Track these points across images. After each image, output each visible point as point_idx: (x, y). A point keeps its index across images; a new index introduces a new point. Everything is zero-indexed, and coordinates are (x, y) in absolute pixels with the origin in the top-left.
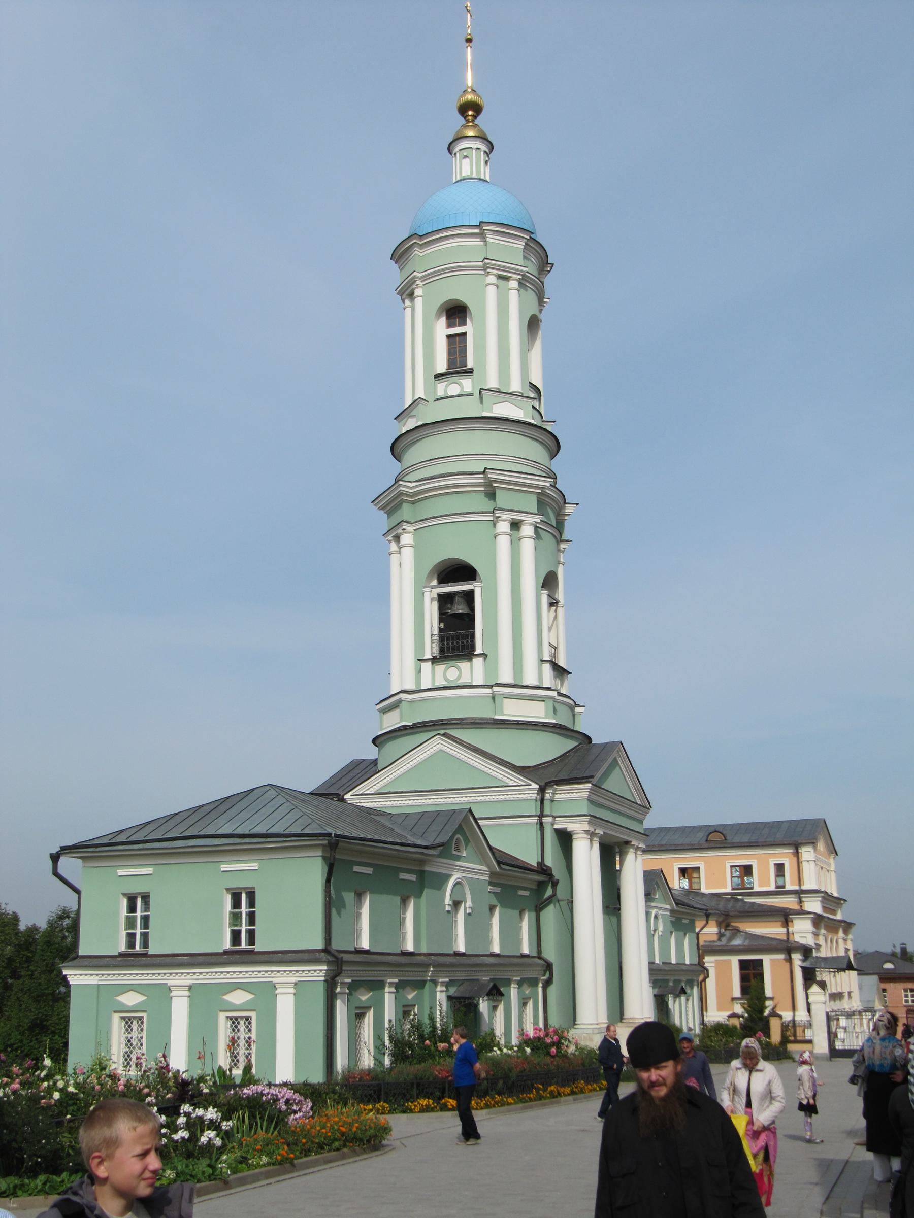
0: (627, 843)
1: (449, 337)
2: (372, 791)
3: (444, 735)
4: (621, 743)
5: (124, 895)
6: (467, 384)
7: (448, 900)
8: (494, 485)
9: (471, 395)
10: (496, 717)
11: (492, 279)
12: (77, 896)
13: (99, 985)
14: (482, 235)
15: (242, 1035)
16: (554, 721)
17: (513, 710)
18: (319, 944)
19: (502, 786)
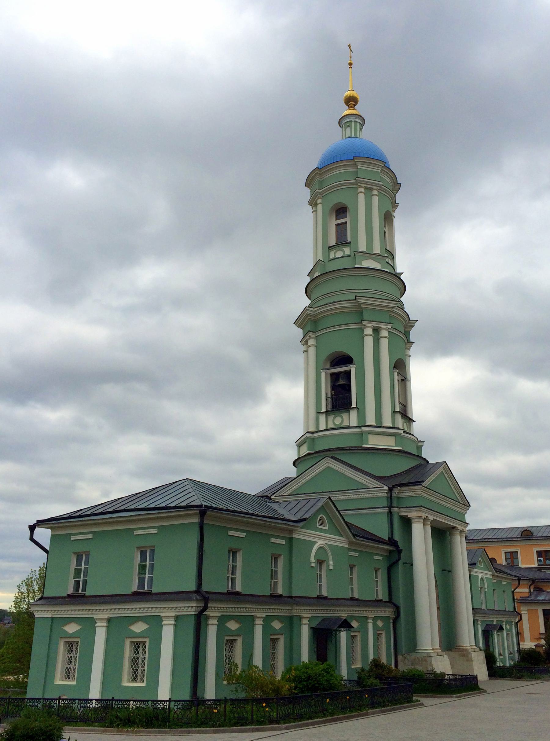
0: (454, 528)
1: (337, 225)
2: (287, 493)
3: (332, 457)
4: (446, 462)
5: (75, 553)
6: (347, 251)
7: (312, 559)
8: (362, 306)
9: (349, 256)
10: (364, 446)
11: (362, 190)
12: (47, 554)
13: (52, 618)
14: (355, 165)
15: (141, 656)
16: (401, 449)
17: (374, 442)
18: (193, 588)
19: (365, 488)
